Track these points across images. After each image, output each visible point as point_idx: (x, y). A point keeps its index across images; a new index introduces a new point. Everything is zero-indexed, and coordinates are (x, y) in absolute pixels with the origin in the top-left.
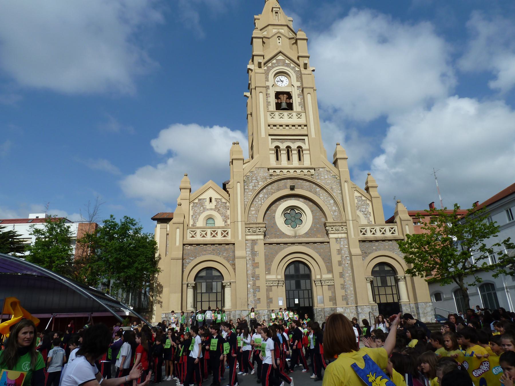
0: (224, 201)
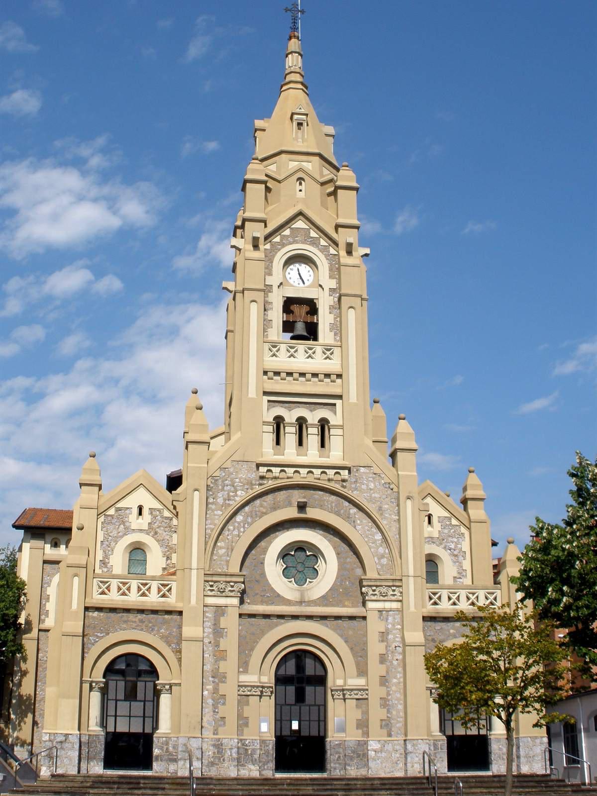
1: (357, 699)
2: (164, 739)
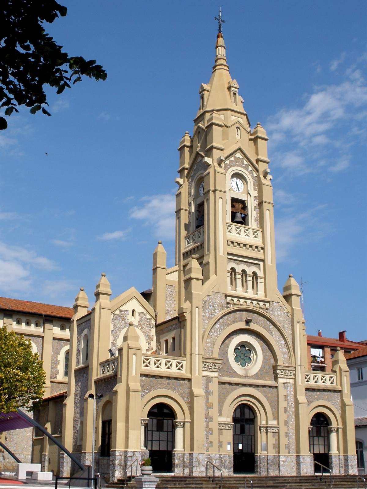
0: (148, 316)
1: (273, 432)
2: (181, 454)
